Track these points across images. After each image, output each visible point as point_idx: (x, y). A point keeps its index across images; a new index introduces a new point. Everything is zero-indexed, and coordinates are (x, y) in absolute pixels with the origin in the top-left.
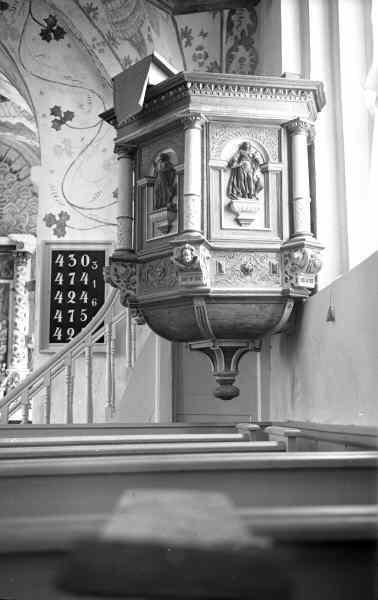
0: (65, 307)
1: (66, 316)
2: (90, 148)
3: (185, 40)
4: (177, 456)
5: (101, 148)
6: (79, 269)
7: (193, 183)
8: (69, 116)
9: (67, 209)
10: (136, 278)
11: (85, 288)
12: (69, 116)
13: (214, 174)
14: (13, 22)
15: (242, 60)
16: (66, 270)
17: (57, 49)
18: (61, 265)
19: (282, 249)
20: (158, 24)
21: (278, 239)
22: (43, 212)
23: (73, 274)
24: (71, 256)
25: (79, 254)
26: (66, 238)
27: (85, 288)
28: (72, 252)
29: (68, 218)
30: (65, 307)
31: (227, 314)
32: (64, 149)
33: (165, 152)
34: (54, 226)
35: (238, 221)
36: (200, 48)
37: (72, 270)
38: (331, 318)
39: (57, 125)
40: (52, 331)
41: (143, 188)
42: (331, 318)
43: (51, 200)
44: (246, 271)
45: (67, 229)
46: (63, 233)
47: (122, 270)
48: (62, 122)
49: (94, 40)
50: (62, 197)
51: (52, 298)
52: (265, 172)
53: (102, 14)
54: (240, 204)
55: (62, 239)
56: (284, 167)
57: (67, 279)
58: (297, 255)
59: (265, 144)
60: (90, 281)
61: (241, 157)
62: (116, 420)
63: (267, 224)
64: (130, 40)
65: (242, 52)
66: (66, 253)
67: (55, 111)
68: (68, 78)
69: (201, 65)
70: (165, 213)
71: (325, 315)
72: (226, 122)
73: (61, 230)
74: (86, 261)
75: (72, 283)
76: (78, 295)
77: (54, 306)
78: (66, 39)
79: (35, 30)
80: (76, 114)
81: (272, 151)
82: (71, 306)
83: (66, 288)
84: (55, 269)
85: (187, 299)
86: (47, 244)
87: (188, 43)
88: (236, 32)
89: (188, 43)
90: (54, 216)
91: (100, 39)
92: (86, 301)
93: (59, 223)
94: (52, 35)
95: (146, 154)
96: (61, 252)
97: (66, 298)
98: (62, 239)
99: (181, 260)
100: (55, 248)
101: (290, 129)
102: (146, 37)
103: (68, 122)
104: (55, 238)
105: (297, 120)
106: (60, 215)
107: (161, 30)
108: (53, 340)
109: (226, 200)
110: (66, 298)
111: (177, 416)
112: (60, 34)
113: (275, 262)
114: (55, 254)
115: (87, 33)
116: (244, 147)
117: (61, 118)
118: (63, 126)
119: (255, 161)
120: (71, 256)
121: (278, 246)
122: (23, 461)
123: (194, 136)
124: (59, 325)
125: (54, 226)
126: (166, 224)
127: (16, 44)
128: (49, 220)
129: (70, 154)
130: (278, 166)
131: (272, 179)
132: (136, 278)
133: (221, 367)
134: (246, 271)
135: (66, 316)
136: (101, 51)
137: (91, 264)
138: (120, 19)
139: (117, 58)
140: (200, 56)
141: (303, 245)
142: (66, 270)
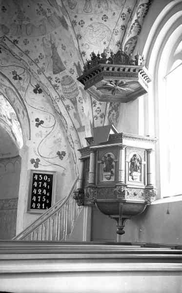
0: (37, 195)
1: (37, 199)
2: (49, 135)
3: (94, 105)
4: (12, 255)
5: (53, 136)
6: (43, 181)
7: (122, 166)
8: (42, 122)
9: (39, 158)
10: (96, 193)
11: (45, 188)
12: (42, 122)
13: (127, 164)
14: (23, 85)
15: (113, 115)
16: (38, 181)
17: (39, 97)
18: (36, 179)
19: (145, 189)
20: (86, 99)
21: (143, 185)
22: (30, 158)
23: (41, 183)
24: (40, 176)
25: (43, 175)
26: (39, 169)
27: (45, 188)
28: (41, 174)
29: (39, 161)
30: (37, 195)
31: (127, 207)
32: (39, 135)
33: (110, 153)
34: (34, 164)
35: (133, 179)
36: (98, 108)
37: (41, 181)
38: (168, 213)
39: (37, 125)
40: (32, 204)
41: (100, 163)
42: (168, 213)
43: (34, 154)
44: (135, 194)
45: (39, 165)
46: (37, 167)
47: (92, 190)
48: (39, 124)
49: (56, 97)
50: (38, 153)
51: (32, 191)
52: (140, 164)
53: (60, 88)
54: (134, 173)
55: (37, 169)
56: (146, 163)
57: (38, 185)
58: (151, 191)
59: (141, 155)
60: (47, 186)
61: (135, 159)
62: (69, 240)
63: (141, 180)
64: (71, 100)
65: (114, 112)
66: (38, 175)
67: (37, 120)
68: (42, 108)
69: (98, 113)
70: (110, 174)
71: (166, 212)
72: (131, 148)
73: (36, 166)
74: (46, 178)
75: (40, 186)
76: (42, 191)
77: (33, 194)
78: (42, 94)
79: (31, 89)
80: (45, 122)
81: (143, 157)
82: (39, 195)
83: (37, 188)
84: (34, 180)
85: (118, 203)
86: (32, 170)
87: (95, 106)
88: (113, 106)
89: (95, 106)
90: (34, 160)
91: (58, 97)
92: (45, 193)
93: (36, 163)
94: (38, 91)
95: (101, 153)
96: (36, 174)
97: (37, 192)
98: (37, 169)
99: (120, 191)
100: (35, 172)
101: (148, 151)
102: (78, 101)
103: (42, 125)
104: (34, 168)
105: (151, 149)
106: (37, 160)
107: (87, 100)
108: (32, 208)
109: (130, 172)
110: (37, 192)
111: (92, 240)
112: (40, 91)
113: (143, 192)
114: (34, 174)
115: (54, 95)
116: (135, 155)
117: (39, 123)
118: (40, 126)
119: (138, 160)
120: (40, 176)
121: (144, 187)
122: (77, 255)
123: (123, 151)
124: (34, 202)
125: (34, 164)
126: (109, 177)
127: (24, 93)
128: (32, 161)
129: (41, 137)
130: (144, 162)
131: (143, 166)
132: (96, 193)
133: (120, 224)
134: (135, 194)
135: (37, 199)
136: (58, 101)
137: (48, 179)
138: (68, 92)
139: (64, 104)
140: (98, 111)
141: (153, 188)
142: (38, 181)
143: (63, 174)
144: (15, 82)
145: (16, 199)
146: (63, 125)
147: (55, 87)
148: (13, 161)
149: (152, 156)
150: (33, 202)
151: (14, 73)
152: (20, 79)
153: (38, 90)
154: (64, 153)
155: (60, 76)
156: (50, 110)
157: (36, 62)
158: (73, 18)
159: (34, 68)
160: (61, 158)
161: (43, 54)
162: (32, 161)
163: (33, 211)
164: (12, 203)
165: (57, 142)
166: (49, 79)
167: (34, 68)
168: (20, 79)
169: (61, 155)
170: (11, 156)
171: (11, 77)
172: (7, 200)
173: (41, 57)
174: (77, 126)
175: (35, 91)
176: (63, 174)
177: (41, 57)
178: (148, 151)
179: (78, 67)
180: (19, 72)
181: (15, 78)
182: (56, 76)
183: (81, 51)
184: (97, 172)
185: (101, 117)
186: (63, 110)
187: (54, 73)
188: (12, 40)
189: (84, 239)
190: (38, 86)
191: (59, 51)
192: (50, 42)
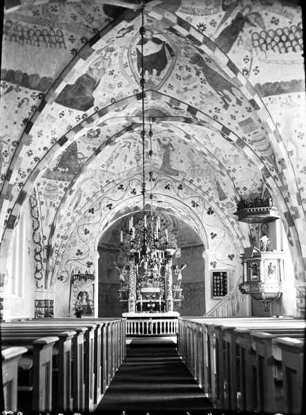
8: (215, 235)
12: (215, 235)
39: (213, 237)
73: (214, 267)
93: (214, 264)
108: (214, 295)
112: (212, 212)
117: (213, 236)
143: (234, 271)
144: (194, 209)
145: (203, 283)
146: (231, 235)
147: (222, 209)
148: (199, 248)
149: (281, 262)
150: (214, 292)
151: (193, 202)
152: (197, 205)
153: (210, 212)
154: (233, 256)
155: (225, 202)
156: (221, 225)
157: (207, 193)
158: (228, 169)
159: (206, 197)
160: (231, 259)
161: (211, 187)
162: (212, 264)
163: (215, 298)
164: (202, 286)
165: (227, 248)
166: (218, 204)
167: (206, 197)
168: (197, 205)
169: (231, 257)
170: (196, 245)
171: (191, 205)
172: (197, 283)
173: (210, 189)
174: (240, 236)
175: (208, 213)
176: (234, 271)
177: (210, 189)
178: (279, 260)
179: (236, 199)
180: (196, 200)
181: (194, 206)
182: (222, 202)
183: (237, 187)
184: (132, 364)
185: (256, 229)
186: (229, 225)
187: (221, 200)
188: (189, 180)
189: (248, 315)
190: (210, 209)
191: (221, 185)
192: (215, 180)
